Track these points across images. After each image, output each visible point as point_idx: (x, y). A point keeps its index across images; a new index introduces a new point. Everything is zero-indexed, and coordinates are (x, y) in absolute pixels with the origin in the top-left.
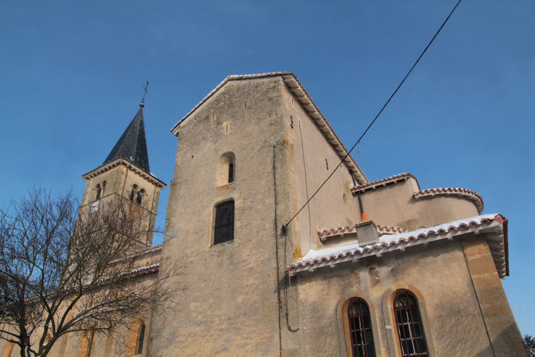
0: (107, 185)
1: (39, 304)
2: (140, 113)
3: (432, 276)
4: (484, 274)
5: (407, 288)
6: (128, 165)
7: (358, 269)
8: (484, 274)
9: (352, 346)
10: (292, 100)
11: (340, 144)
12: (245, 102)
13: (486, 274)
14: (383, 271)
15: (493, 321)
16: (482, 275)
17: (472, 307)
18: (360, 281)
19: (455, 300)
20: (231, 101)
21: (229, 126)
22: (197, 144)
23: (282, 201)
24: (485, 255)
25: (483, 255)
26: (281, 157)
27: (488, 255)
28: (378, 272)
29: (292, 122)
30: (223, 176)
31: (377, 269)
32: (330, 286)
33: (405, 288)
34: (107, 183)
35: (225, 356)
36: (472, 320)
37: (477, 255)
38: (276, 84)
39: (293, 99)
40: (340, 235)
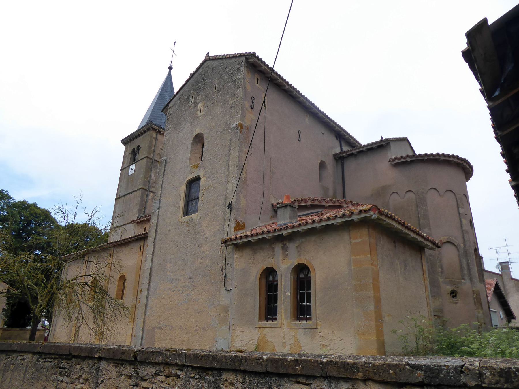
0: (141, 150)
1: (415, 230)
2: (170, 73)
3: (324, 254)
4: (360, 256)
5: (305, 262)
6: (157, 130)
7: (275, 244)
8: (360, 256)
9: (266, 305)
10: (258, 79)
11: (320, 113)
12: (216, 84)
13: (362, 256)
14: (292, 246)
15: (359, 295)
16: (359, 257)
17: (347, 283)
18: (275, 254)
19: (336, 276)
20: (206, 83)
21: (202, 108)
22: (179, 124)
23: (232, 181)
24: (364, 239)
25: (362, 239)
26: (235, 139)
27: (366, 239)
28: (287, 247)
29: (253, 103)
30: (196, 155)
31: (287, 244)
32: (254, 256)
33: (304, 263)
34: (141, 147)
35: (518, 350)
36: (345, 293)
37: (358, 239)
38: (240, 66)
39: (259, 78)
40: (324, 205)
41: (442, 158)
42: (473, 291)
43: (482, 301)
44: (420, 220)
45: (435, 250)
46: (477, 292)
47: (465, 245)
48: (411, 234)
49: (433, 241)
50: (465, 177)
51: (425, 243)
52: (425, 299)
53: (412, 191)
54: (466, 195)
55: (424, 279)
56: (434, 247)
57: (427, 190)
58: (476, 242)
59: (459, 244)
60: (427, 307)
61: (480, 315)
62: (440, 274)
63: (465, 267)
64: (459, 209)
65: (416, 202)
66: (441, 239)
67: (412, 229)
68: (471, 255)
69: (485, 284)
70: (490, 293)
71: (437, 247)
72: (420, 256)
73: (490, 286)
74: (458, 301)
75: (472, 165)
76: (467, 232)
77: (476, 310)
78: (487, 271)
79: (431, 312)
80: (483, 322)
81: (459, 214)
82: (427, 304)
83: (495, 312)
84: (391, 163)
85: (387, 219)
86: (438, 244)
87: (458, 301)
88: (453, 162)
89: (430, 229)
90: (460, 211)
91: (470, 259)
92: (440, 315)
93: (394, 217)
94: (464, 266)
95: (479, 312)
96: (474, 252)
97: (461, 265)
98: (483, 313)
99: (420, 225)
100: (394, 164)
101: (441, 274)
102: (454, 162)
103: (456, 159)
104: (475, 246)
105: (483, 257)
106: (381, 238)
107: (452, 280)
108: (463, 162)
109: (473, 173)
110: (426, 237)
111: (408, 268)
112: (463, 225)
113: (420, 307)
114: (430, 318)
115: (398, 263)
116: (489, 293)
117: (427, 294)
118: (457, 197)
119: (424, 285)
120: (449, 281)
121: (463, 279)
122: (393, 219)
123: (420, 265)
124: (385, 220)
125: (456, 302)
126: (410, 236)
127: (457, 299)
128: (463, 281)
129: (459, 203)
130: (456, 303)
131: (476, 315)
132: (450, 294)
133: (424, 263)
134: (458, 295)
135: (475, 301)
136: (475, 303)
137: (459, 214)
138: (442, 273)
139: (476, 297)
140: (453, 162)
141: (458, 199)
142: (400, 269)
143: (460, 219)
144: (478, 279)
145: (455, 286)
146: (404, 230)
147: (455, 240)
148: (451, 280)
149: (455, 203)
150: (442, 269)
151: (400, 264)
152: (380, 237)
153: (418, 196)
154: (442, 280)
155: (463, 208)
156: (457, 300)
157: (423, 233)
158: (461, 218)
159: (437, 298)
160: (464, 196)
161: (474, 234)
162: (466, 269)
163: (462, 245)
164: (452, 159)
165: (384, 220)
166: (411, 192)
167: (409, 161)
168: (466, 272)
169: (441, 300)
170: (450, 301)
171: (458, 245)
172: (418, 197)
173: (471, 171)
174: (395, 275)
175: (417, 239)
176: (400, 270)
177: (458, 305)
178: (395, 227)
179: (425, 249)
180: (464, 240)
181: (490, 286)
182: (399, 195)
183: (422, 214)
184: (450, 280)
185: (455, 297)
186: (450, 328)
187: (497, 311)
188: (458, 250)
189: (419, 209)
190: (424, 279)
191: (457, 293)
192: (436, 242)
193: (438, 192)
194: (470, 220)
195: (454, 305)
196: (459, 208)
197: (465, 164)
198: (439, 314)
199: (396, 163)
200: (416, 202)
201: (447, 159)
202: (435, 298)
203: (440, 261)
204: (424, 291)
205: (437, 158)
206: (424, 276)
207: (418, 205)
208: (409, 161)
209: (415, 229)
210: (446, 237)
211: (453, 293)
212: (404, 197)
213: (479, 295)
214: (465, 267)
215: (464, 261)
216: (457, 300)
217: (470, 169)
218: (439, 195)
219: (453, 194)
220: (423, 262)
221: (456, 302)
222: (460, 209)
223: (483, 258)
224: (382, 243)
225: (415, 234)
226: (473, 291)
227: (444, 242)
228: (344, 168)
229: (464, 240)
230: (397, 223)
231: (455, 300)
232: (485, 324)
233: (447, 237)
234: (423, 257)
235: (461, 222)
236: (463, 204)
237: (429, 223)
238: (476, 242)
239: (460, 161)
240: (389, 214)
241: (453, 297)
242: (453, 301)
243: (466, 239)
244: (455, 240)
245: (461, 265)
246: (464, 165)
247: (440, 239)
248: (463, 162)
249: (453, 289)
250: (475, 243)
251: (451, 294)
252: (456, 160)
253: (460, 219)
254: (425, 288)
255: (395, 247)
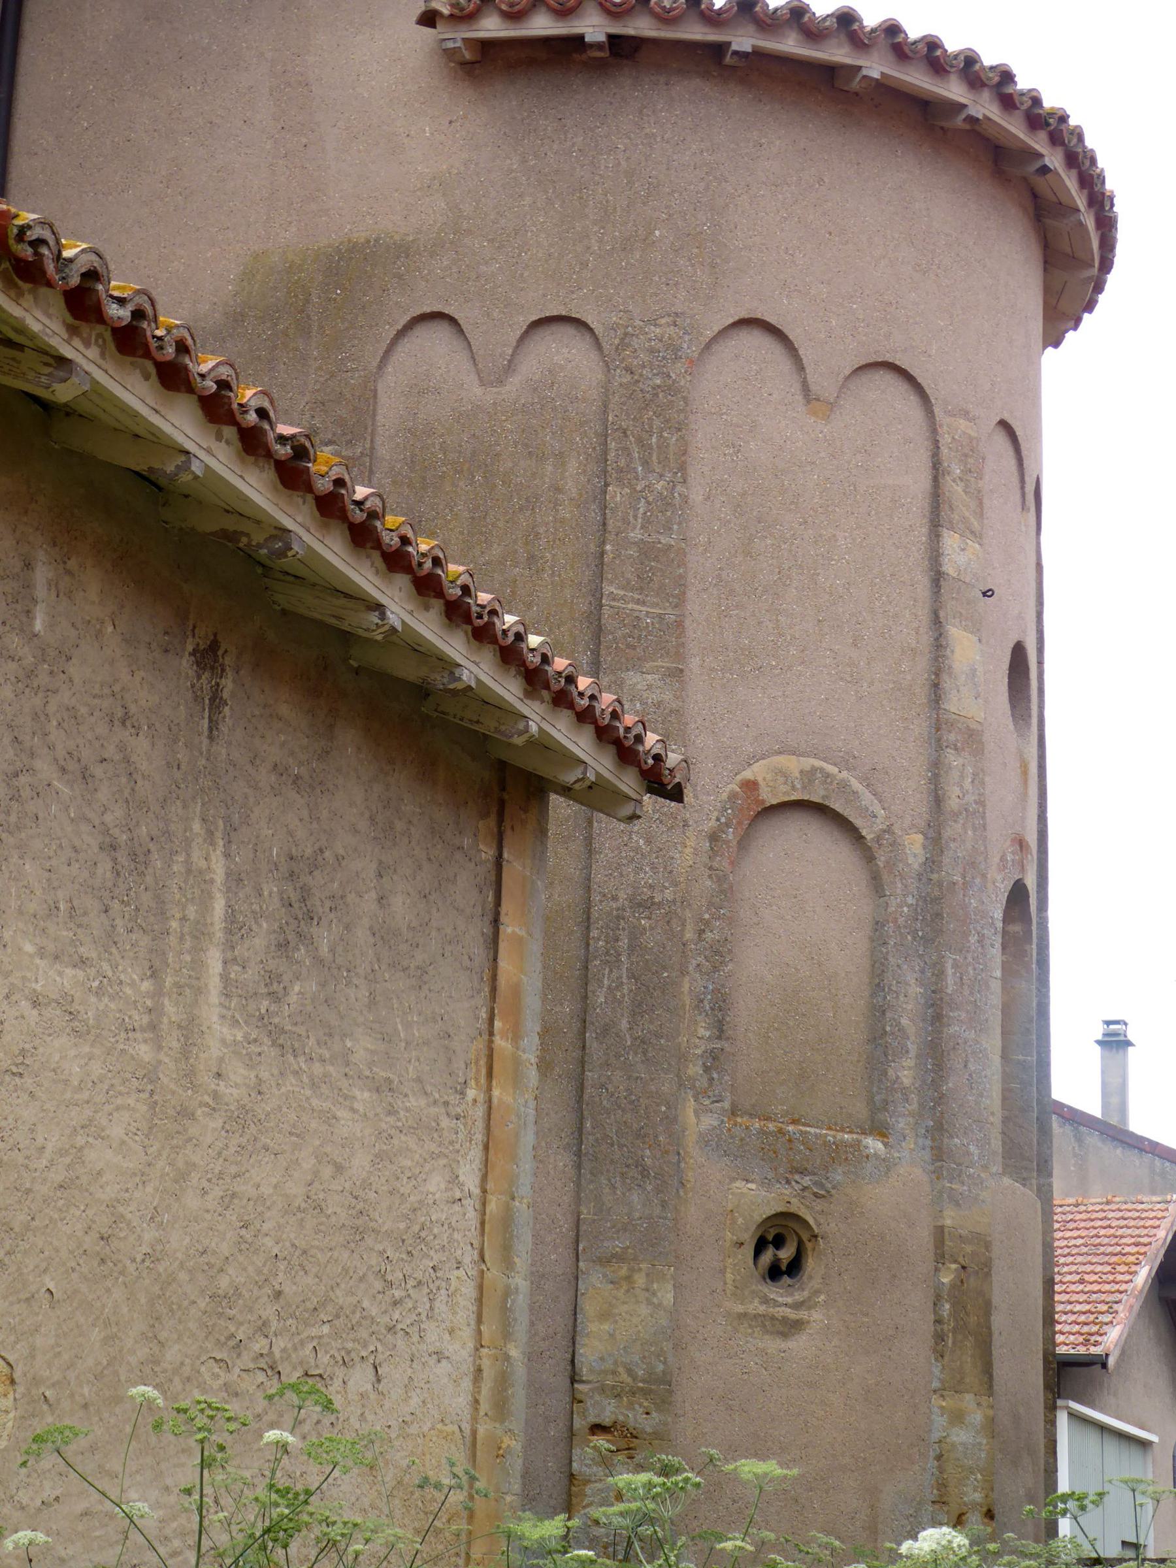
41: (875, 67)
42: (940, 1233)
43: (998, 1321)
44: (608, 589)
45: (634, 817)
46: (969, 1249)
47: (935, 842)
48: (383, 600)
49: (615, 715)
50: (1047, 290)
51: (534, 728)
52: (469, 1256)
53: (579, 324)
54: (1019, 433)
55: (490, 1075)
56: (628, 782)
57: (709, 334)
58: (1032, 839)
59: (889, 830)
60: (467, 1333)
61: (961, 1436)
62: (695, 1069)
63: (911, 1030)
64: (938, 536)
65: (605, 422)
66: (757, 771)
67: (391, 540)
68: (973, 939)
69: (1045, 1195)
70: (1124, 1297)
71: (650, 790)
72: (487, 853)
73: (1134, 1249)
74: (803, 1314)
75: (1109, 186)
76: (973, 739)
77: (940, 1392)
78: (1142, 1139)
79: (503, 1381)
80: (977, 1496)
81: (937, 578)
82: (480, 1300)
83: (1144, 1444)
84: (442, 31)
85: (93, 352)
86: (658, 758)
87: (803, 1314)
88: (959, 121)
89: (677, 674)
90: (945, 560)
91: (956, 966)
92: (646, 1424)
93: (466, 590)
94: (904, 1021)
95: (957, 1418)
96: (998, 914)
97: (878, 1012)
98: (991, 1427)
99: (598, 631)
100: (468, 56)
101: (707, 1069)
102: (972, 120)
103: (986, 95)
104: (1023, 869)
105: (1131, 1037)
106: (42, 574)
107: (791, 1128)
108: (1039, 143)
109: (1106, 265)
110: (545, 659)
111: (324, 938)
112: (944, 676)
113: (391, 1329)
114: (482, 1430)
115: (219, 869)
116: (1118, 1296)
117: (493, 1206)
118: (945, 439)
119: (480, 1125)
120: (762, 1132)
121: (881, 1131)
122: (562, 699)
123: (474, 933)
124: (67, 352)
125: (785, 1320)
126: (374, 618)
127: (798, 1296)
128: (874, 1145)
129: (954, 489)
130: (791, 1327)
131: (936, 1435)
132: (749, 1250)
133: (510, 928)
134: (811, 1264)
135: (938, 1321)
136: (940, 1337)
137: (937, 578)
138: (713, 1062)
139: (953, 1286)
140: (959, 121)
141: (944, 451)
142: (229, 932)
143: (937, 621)
144: (996, 1144)
145: (807, 1181)
146: (306, 537)
147: (867, 798)
148: (780, 1131)
149: (918, 483)
150: (720, 1030)
151: (235, 879)
152: (28, 565)
153: (629, 370)
154: (709, 1121)
155: (977, 536)
156: (797, 1306)
157: (534, 640)
158: (942, 614)
159: (640, 1280)
160: (1001, 441)
161: (1025, 773)
162: (912, 1048)
163: (914, 846)
164: (954, 90)
165: (62, 361)
166: (569, 330)
167: (602, 38)
168: (905, 1072)
169: (667, 1296)
170: (740, 1309)
171: (878, 839)
172: (627, 378)
173: (1095, 244)
174: (154, 974)
175: (450, 666)
176: (219, 935)
177: (798, 1344)
178: (196, 467)
179: (553, 797)
180: (937, 800)
181: (1134, 1249)
182: (466, 339)
183: (636, 535)
184: (771, 1126)
185: (786, 1280)
186: (773, 1556)
187: (1153, 1438)
188: (877, 884)
189: (617, 494)
190: (490, 1075)
191: (809, 1245)
192: (639, 739)
193: (799, 365)
194: (1019, 652)
195: (773, 1345)
196: (945, 533)
197: (1054, 160)
198: (635, 1417)
199: (487, 47)
200: (605, 422)
201: (918, 79)
202: (624, 1272)
203: (719, 955)
204: (470, 1179)
205: (837, 53)
206: (499, 1041)
207: (611, 455)
208: (602, 38)
209: (424, 548)
210: (794, 765)
211: (779, 1242)
212: (510, 367)
213: (986, 1269)
214: (911, 1030)
215: (911, 978)
216: (797, 1306)
217: (1090, 222)
218: (799, 397)
219: (914, 399)
220: (504, 909)
221: (792, 1314)
222: (951, 541)
223: (1128, 1043)
224: (38, 626)
225: (427, 608)
226: (940, 1233)
227: (774, 802)
228: (27, 27)
229: (937, 800)
230: (219, 437)
231: (780, 1295)
232: (990, 1515)
233: (809, 762)
234: (516, 867)
235: (939, 645)
236: (981, 504)
237: (679, 624)
238: (1032, 839)
239: (1015, 127)
240: (121, 301)
241: (775, 1273)
242: (762, 1309)
243: (953, 802)
244: (867, 798)
245: (878, 1012)
246: (1045, 170)
247: (748, 774)
248: (1039, 143)
249: (781, 1208)
250: (1021, 843)
251: (760, 1246)
252: (984, 107)
253: (937, 621)
254: (486, 1148)
255: (216, 701)
